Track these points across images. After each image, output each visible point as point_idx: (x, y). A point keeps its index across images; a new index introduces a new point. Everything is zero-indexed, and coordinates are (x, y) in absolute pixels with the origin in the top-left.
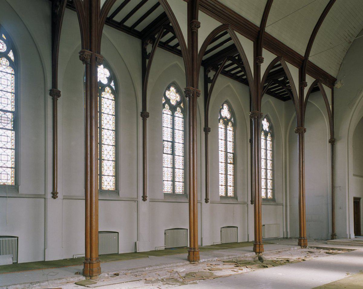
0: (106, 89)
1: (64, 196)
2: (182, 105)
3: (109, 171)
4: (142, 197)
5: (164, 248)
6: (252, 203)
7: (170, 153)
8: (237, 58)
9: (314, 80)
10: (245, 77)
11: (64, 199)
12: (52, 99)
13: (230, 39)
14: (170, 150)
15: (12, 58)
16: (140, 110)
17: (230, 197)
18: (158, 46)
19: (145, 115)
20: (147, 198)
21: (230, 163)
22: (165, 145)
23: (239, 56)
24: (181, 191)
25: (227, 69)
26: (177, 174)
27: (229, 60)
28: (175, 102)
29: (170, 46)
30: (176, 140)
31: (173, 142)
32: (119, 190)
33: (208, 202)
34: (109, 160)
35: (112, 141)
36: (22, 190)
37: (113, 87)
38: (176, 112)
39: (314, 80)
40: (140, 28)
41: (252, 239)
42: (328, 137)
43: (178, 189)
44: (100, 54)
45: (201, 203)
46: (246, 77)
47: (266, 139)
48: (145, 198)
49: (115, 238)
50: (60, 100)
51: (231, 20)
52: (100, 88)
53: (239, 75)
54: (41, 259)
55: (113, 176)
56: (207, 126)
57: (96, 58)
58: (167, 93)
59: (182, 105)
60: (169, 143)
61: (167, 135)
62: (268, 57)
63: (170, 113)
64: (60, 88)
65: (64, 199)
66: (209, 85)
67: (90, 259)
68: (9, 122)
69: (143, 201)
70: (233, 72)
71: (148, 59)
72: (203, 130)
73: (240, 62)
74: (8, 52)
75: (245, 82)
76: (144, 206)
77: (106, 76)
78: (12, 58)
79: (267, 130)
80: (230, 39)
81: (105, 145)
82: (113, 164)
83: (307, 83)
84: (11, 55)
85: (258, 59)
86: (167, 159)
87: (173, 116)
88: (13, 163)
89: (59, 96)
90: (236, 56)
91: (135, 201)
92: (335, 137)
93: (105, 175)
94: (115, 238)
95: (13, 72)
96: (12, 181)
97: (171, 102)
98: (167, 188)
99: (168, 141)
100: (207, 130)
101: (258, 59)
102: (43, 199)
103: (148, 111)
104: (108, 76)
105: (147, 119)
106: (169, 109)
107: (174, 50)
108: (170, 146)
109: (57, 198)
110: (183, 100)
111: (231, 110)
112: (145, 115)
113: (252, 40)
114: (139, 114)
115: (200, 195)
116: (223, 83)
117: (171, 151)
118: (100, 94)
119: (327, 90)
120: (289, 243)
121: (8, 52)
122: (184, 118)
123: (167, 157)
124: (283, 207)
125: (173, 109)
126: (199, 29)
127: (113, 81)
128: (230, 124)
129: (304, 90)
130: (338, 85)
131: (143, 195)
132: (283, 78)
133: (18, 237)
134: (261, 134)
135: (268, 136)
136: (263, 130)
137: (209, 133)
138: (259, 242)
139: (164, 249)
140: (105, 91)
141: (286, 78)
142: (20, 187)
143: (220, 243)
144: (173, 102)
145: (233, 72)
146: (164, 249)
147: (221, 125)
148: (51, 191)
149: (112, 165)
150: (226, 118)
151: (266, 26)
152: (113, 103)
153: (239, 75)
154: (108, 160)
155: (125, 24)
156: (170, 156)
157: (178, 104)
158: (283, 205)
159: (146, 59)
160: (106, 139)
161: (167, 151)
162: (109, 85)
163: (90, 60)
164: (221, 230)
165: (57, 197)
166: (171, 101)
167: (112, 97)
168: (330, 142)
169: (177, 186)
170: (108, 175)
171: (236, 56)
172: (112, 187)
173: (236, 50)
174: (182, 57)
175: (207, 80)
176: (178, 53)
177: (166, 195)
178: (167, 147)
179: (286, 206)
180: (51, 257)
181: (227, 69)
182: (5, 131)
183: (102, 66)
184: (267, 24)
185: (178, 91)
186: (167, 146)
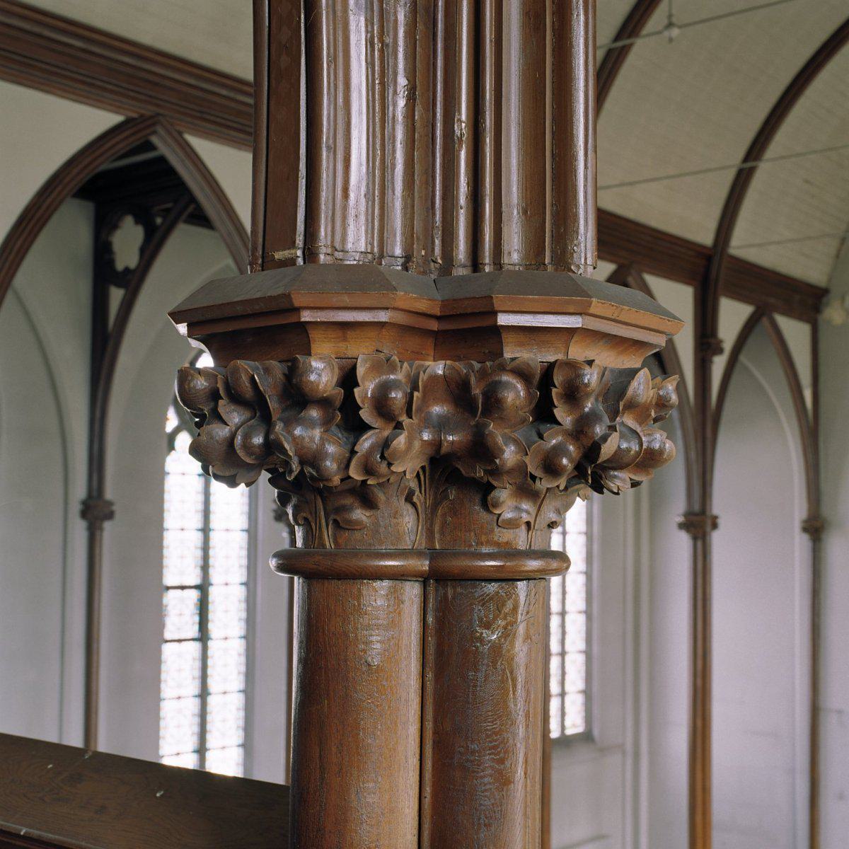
16: (79, 491)
19: (95, 511)
42: (799, 511)
61: (179, 564)
71: (119, 285)
83: (721, 341)
86: (178, 664)
92: (826, 511)
105: (107, 525)
112: (95, 511)
114: (76, 508)
119: (795, 332)
120: (583, 250)
130: (834, 314)
168: (805, 530)
178: (179, 613)
179: (637, 755)
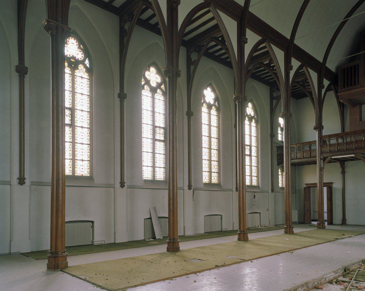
0: (80, 67)
1: (32, 182)
2: (163, 87)
4: (18, 179)
6: (237, 191)
8: (220, 39)
9: (300, 64)
10: (229, 60)
12: (19, 76)
13: (213, 19)
15: (88, 66)
17: (214, 184)
18: (250, 77)
19: (122, 96)
21: (160, 141)
23: (222, 37)
24: (163, 178)
25: (210, 51)
27: (211, 41)
29: (150, 24)
33: (192, 189)
37: (217, 105)
38: (156, 95)
39: (300, 64)
41: (47, 246)
44: (67, 26)
45: (11, 185)
46: (230, 60)
47: (250, 125)
48: (123, 184)
50: (27, 78)
51: (268, 33)
52: (73, 66)
53: (223, 57)
54: (113, 242)
56: (190, 110)
57: (63, 29)
58: (147, 73)
59: (163, 87)
62: (252, 38)
63: (150, 94)
64: (27, 63)
66: (192, 67)
67: (55, 253)
70: (217, 54)
73: (223, 41)
74: (84, 60)
75: (227, 63)
76: (122, 194)
78: (88, 66)
79: (212, 102)
80: (213, 19)
84: (87, 62)
85: (242, 40)
90: (219, 37)
95: (88, 77)
97: (151, 84)
98: (205, 180)
99: (160, 127)
100: (190, 114)
101: (242, 40)
102: (183, 191)
103: (125, 92)
106: (150, 91)
107: (155, 29)
109: (24, 185)
110: (163, 81)
111: (255, 108)
112: (122, 96)
113: (283, 51)
115: (182, 181)
116: (206, 65)
124: (233, 192)
125: (153, 90)
126: (246, 45)
128: (253, 121)
129: (290, 73)
131: (189, 184)
132: (268, 62)
133: (92, 222)
134: (245, 119)
135: (252, 121)
136: (205, 102)
138: (173, 239)
140: (78, 69)
141: (271, 61)
145: (217, 54)
150: (73, 57)
151: (250, 6)
153: (223, 57)
157: (159, 86)
158: (269, 193)
159: (124, 38)
163: (58, 33)
164: (144, 221)
165: (25, 183)
166: (151, 83)
171: (219, 37)
173: (220, 31)
174: (161, 36)
175: (189, 62)
177: (205, 184)
180: (120, 239)
181: (210, 51)
183: (209, 89)
184: (296, 37)
185: (159, 72)
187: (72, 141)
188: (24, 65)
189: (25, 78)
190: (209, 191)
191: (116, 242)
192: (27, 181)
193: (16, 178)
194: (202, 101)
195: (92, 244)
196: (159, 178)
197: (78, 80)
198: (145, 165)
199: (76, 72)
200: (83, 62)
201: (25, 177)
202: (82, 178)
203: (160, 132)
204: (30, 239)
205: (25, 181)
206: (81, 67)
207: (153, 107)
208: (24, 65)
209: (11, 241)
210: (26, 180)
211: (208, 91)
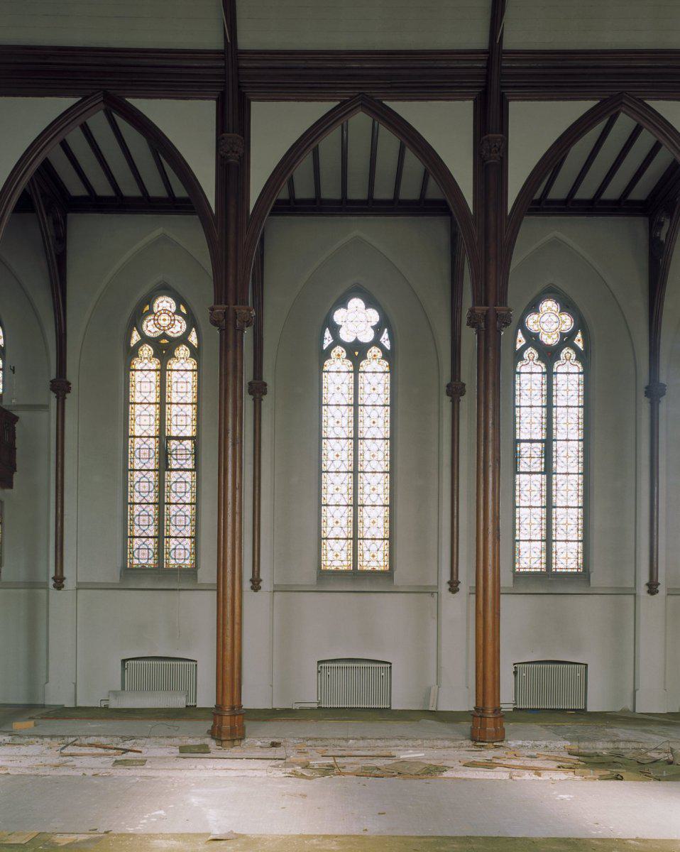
3: (375, 530)
4: (449, 583)
5: (512, 706)
7: (538, 470)
11: (274, 591)
12: (650, 403)
14: (539, 462)
20: (659, 588)
22: (522, 453)
26: (562, 522)
28: (555, 336)
29: (606, 202)
30: (559, 434)
31: (548, 442)
32: (590, 570)
34: (375, 506)
35: (382, 463)
36: (597, 580)
40: (640, 193)
43: (564, 561)
45: (635, 595)
49: (578, 675)
52: (357, 353)
55: (384, 539)
56: (261, 378)
60: (534, 445)
65: (274, 591)
68: (188, 456)
69: (450, 594)
72: (445, 393)
74: (187, 333)
77: (370, 324)
81: (366, 474)
82: (384, 512)
84: (328, 339)
87: (550, 374)
88: (193, 528)
89: (462, 393)
91: (432, 593)
93: (365, 539)
94: (524, 675)
96: (386, 563)
98: (530, 558)
104: (374, 323)
108: (539, 453)
114: (444, 389)
117: (543, 466)
118: (321, 365)
121: (187, 333)
122: (198, 370)
123: (530, 481)
125: (549, 355)
127: (386, 330)
133: (586, 665)
136: (337, 341)
137: (461, 398)
139: (512, 710)
142: (592, 575)
143: (315, 706)
144: (550, 337)
146: (512, 710)
147: (146, 360)
148: (448, 579)
149: (382, 515)
152: (386, 379)
154: (372, 506)
155: (578, 196)
156: (540, 479)
157: (566, 339)
160: (333, 461)
161: (530, 466)
162: (376, 342)
165: (63, 586)
167: (577, 368)
169: (559, 554)
170: (373, 537)
172: (382, 564)
176: (559, 210)
178: (530, 457)
182: (181, 473)
186: (529, 453)
187: (390, 503)
188: (65, 377)
189: (262, 402)
190: (418, 595)
191: (439, 710)
192: (266, 585)
193: (645, 583)
194: (166, 341)
195: (584, 710)
196: (562, 566)
197: (560, 380)
198: (573, 543)
199: (364, 364)
200: (183, 340)
201: (261, 577)
202: (373, 574)
203: (533, 453)
204: (468, 687)
205: (261, 584)
206: (183, 351)
207: (549, 395)
208: (65, 375)
209: (635, 692)
210: (65, 581)
211: (349, 311)
